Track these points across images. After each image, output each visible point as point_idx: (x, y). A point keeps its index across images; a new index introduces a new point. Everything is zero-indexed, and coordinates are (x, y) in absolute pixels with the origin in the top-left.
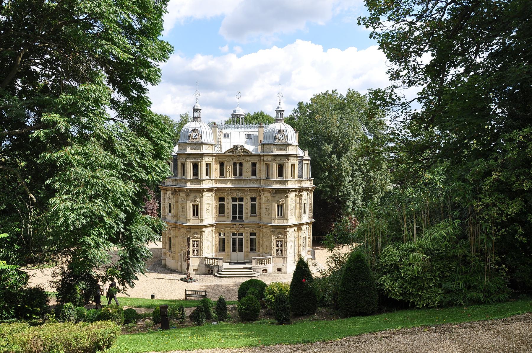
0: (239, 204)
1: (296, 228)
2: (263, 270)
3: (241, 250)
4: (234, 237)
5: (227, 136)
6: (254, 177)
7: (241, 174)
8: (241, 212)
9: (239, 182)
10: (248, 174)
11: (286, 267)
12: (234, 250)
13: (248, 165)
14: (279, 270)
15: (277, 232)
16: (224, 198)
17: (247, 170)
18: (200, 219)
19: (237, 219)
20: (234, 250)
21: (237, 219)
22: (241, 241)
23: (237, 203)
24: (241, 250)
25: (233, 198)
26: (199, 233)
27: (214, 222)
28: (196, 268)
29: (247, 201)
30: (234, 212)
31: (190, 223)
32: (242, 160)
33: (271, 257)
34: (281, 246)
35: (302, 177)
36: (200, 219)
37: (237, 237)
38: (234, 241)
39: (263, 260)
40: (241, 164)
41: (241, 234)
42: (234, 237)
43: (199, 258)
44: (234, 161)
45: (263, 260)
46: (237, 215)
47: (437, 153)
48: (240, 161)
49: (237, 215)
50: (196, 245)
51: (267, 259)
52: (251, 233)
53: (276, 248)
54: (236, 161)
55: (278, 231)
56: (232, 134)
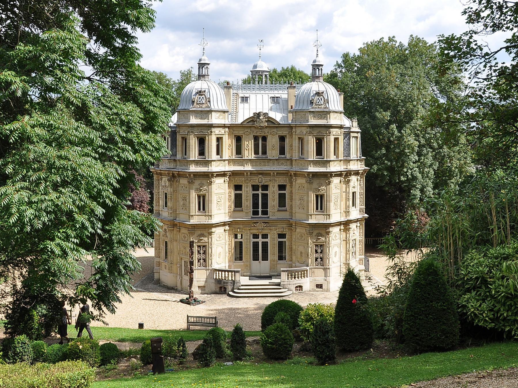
1: (342, 227)
2: (297, 287)
6: (283, 156)
7: (264, 152)
10: (274, 152)
11: (328, 283)
13: (274, 140)
14: (319, 286)
18: (326, 215)
28: (202, 284)
31: (194, 221)
33: (308, 268)
35: (349, 155)
39: (296, 272)
41: (265, 236)
45: (296, 272)
46: (260, 210)
49: (260, 210)
50: (202, 252)
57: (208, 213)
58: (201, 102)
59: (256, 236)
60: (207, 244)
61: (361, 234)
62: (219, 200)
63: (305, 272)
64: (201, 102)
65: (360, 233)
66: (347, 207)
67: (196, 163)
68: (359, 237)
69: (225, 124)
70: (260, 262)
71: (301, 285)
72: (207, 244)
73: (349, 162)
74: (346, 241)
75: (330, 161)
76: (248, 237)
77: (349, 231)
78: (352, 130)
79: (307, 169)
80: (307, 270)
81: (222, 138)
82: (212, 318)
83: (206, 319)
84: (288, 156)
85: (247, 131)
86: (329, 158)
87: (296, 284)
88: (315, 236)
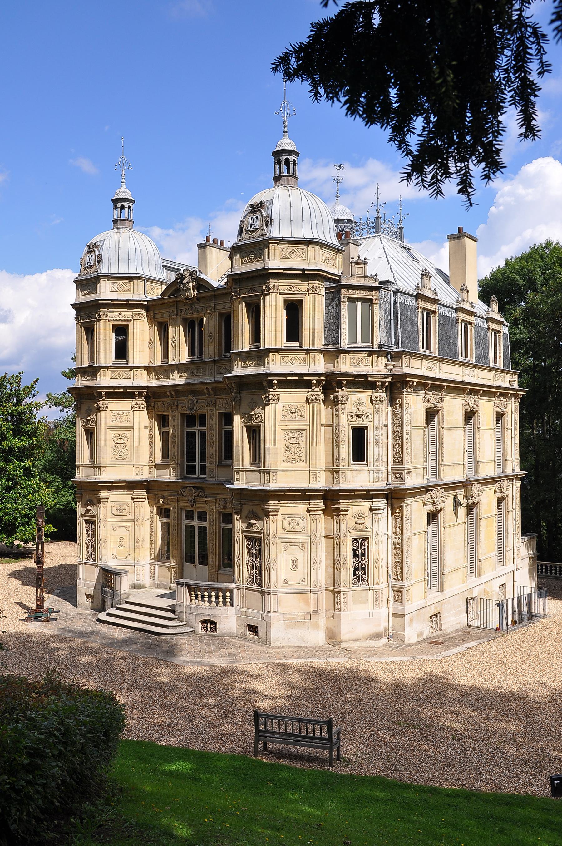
1: (320, 504)
7: (201, 353)
11: (268, 625)
14: (253, 629)
15: (246, 509)
18: (264, 472)
23: (196, 429)
26: (260, 514)
27: (144, 475)
28: (91, 591)
31: (240, 483)
33: (233, 586)
35: (337, 341)
36: (96, 467)
39: (221, 590)
43: (96, 566)
45: (206, 590)
47: (549, 253)
50: (254, 551)
51: (217, 590)
57: (264, 467)
60: (262, 535)
61: (398, 529)
63: (228, 594)
65: (396, 527)
66: (335, 460)
67: (245, 356)
68: (394, 536)
72: (262, 535)
73: (338, 357)
74: (333, 538)
75: (269, 351)
77: (338, 516)
78: (343, 282)
79: (231, 371)
80: (231, 591)
81: (300, 302)
82: (321, 723)
83: (317, 727)
86: (269, 344)
87: (200, 615)
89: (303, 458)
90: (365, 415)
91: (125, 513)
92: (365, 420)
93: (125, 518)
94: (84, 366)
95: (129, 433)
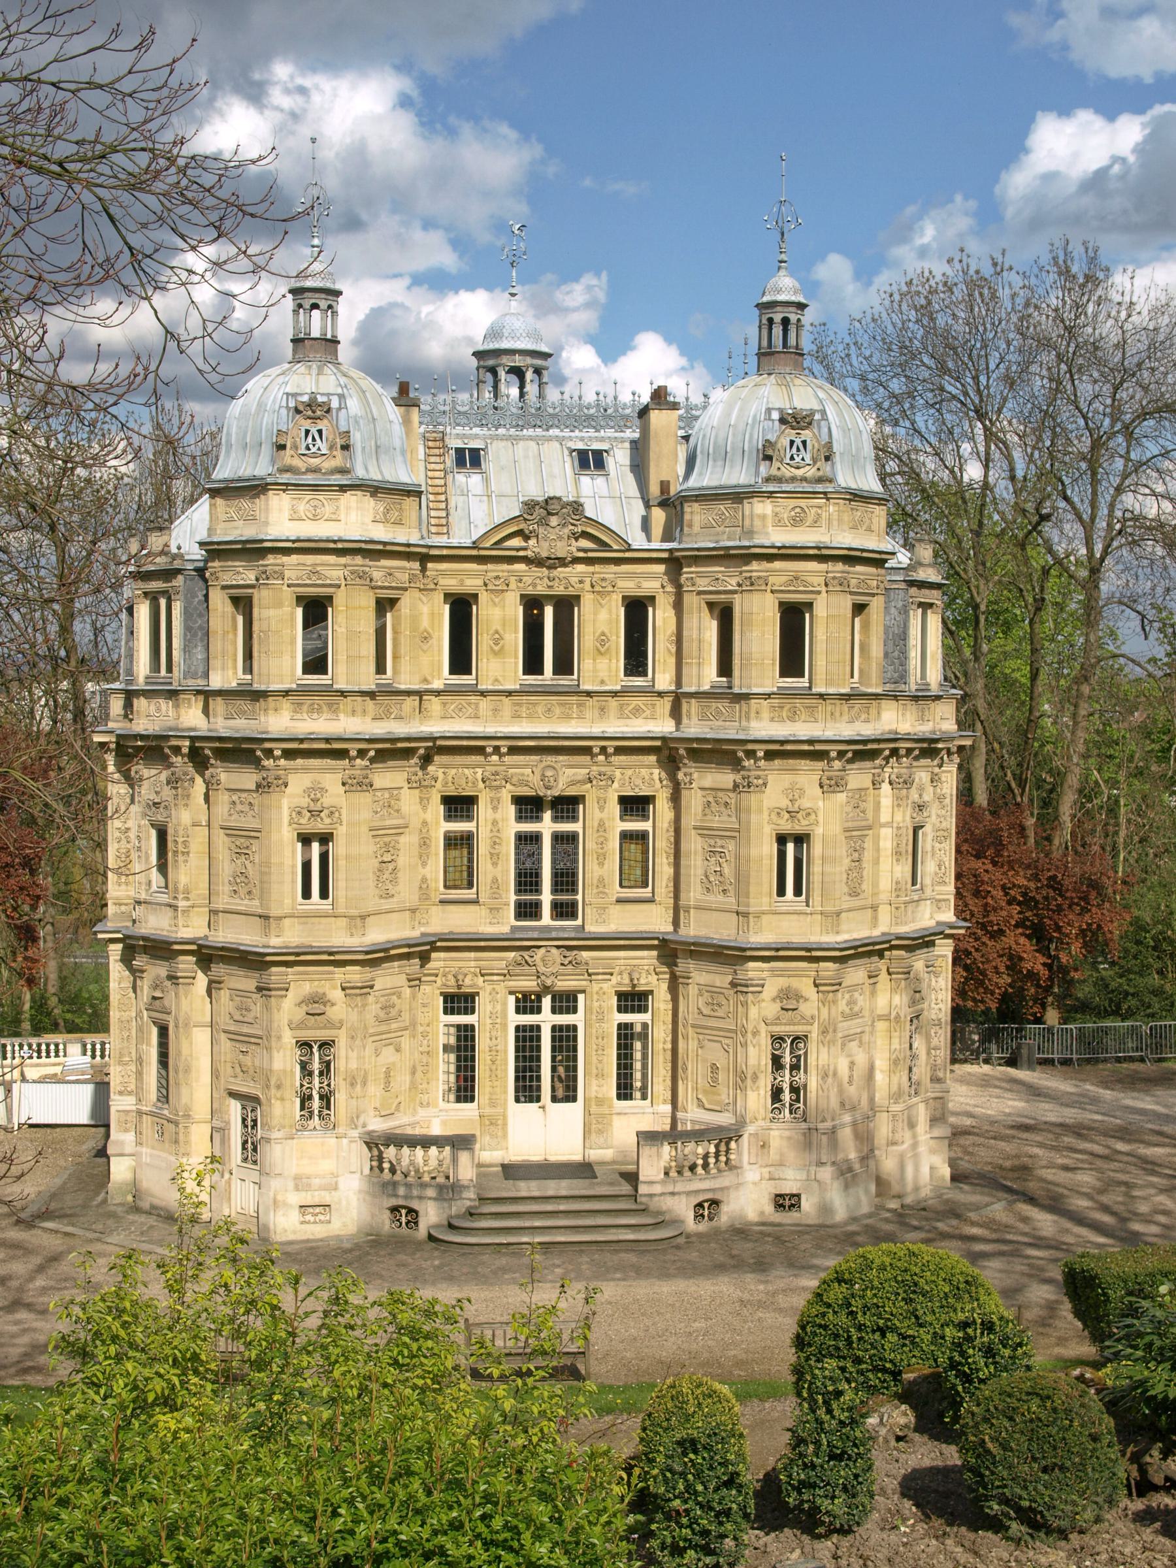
0: (558, 838)
2: (700, 1205)
3: (567, 1092)
4: (528, 1019)
5: (470, 459)
6: (638, 681)
7: (564, 665)
8: (565, 880)
9: (558, 711)
10: (602, 663)
12: (527, 1090)
13: (603, 615)
16: (471, 801)
17: (603, 639)
19: (546, 918)
20: (527, 1090)
21: (546, 918)
22: (565, 1039)
24: (567, 1092)
25: (518, 801)
29: (598, 815)
30: (527, 880)
32: (572, 578)
34: (795, 1067)
37: (547, 1019)
38: (527, 1039)
40: (566, 606)
41: (566, 1002)
42: (528, 1019)
44: (530, 591)
46: (546, 897)
48: (559, 590)
49: (546, 897)
52: (621, 996)
53: (579, 897)
54: (541, 589)
55: (782, 982)
56: (497, 454)
58: (313, 450)
59: (528, 1003)
62: (387, 857)
64: (313, 450)
69: (409, 545)
70: (543, 1107)
71: (717, 1196)
76: (499, 1007)
84: (664, 680)
85: (497, 578)
87: (697, 1192)
88: (774, 1000)
89: (864, 887)
90: (326, 812)
91: (394, 1012)
92: (804, 822)
93: (394, 1026)
94: (702, 689)
95: (402, 839)
